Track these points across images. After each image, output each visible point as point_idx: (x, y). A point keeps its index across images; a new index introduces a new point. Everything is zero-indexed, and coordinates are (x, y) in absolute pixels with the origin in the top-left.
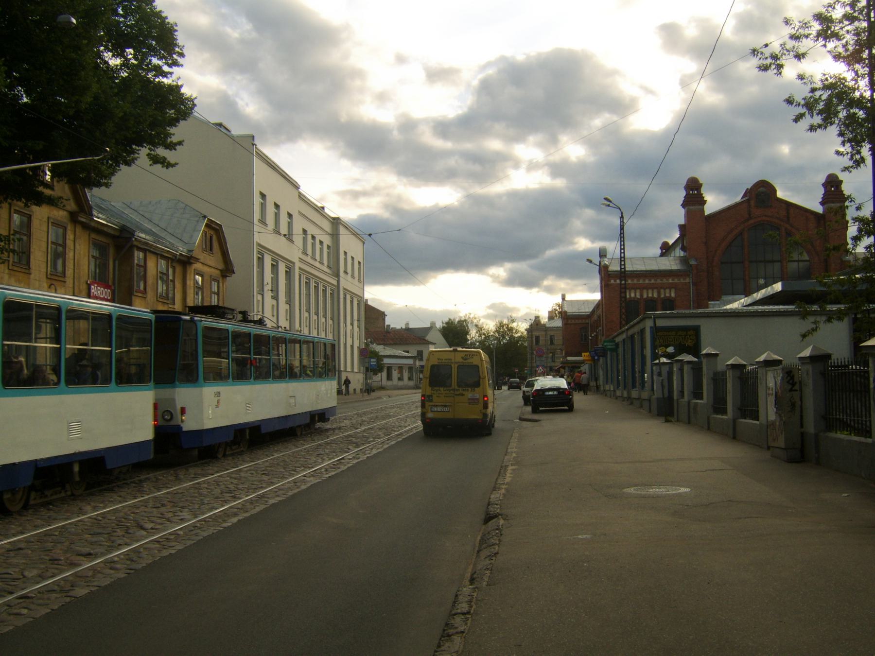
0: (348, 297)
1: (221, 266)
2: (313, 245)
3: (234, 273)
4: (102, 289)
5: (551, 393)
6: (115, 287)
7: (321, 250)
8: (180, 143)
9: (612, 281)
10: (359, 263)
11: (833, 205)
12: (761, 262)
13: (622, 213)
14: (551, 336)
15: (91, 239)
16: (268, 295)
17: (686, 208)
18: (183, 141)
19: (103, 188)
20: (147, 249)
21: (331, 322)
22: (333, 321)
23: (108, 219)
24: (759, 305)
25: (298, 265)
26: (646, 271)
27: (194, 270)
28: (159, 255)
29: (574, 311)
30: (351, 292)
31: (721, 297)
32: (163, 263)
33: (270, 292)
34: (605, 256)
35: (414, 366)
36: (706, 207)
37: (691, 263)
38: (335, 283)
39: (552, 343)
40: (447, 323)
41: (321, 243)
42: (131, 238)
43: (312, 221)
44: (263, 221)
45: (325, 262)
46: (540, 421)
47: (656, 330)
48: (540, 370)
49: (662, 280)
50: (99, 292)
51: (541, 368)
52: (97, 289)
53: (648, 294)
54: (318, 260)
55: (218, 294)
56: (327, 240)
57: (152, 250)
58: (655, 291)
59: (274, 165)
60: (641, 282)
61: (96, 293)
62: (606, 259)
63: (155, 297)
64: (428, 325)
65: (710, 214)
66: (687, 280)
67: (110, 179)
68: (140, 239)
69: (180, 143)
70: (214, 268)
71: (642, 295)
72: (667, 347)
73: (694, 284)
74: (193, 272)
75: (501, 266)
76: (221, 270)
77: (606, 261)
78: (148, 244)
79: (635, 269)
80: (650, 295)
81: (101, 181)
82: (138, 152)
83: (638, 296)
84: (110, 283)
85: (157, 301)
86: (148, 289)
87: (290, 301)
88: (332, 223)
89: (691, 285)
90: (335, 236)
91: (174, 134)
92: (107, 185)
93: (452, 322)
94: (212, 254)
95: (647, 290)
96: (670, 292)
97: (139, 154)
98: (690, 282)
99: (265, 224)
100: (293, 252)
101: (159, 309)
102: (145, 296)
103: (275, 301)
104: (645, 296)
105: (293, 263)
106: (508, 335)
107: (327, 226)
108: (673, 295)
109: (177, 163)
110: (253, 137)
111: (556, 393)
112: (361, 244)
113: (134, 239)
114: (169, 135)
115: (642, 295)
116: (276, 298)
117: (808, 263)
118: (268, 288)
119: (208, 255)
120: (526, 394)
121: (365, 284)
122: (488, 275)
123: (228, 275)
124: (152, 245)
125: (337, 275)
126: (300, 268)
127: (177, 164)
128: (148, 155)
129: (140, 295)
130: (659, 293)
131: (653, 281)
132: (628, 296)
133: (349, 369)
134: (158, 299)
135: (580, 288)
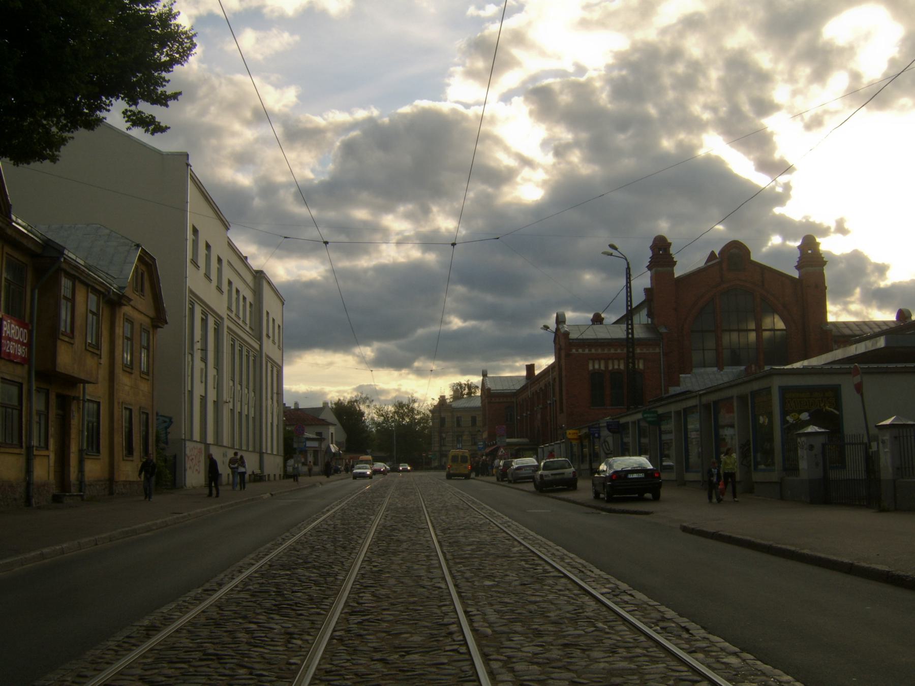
0: (269, 365)
1: (152, 313)
2: (238, 299)
3: (166, 323)
4: (17, 327)
5: (635, 476)
6: (32, 327)
7: (244, 306)
8: (175, 96)
9: (574, 351)
10: (279, 326)
13: (628, 264)
14: (458, 418)
15: (5, 255)
16: (198, 355)
17: (654, 270)
18: (180, 93)
19: (47, 162)
20: (78, 276)
21: (252, 394)
22: (255, 392)
23: (29, 228)
25: (227, 323)
26: (612, 339)
27: (124, 314)
28: (92, 287)
29: (505, 388)
30: (274, 361)
31: (692, 370)
32: (93, 298)
33: (200, 351)
34: (564, 322)
35: (319, 449)
36: (675, 268)
37: (660, 331)
38: (257, 347)
39: (459, 425)
40: (335, 404)
41: (244, 298)
42: (59, 258)
43: (237, 272)
44: (195, 263)
45: (248, 322)
46: (652, 513)
47: (784, 390)
48: (502, 452)
50: (13, 331)
51: (502, 449)
52: (10, 326)
53: (594, 366)
54: (242, 319)
55: (148, 349)
56: (250, 297)
57: (82, 278)
58: (622, 362)
59: (206, 194)
60: (606, 351)
61: (8, 332)
62: (565, 326)
63: (84, 345)
64: (321, 406)
66: (657, 350)
67: (58, 150)
68: (70, 260)
69: (175, 96)
70: (144, 314)
71: (606, 367)
72: (800, 412)
74: (122, 316)
75: (369, 345)
76: (152, 319)
77: (566, 328)
78: (79, 268)
79: (599, 337)
80: (616, 367)
81: (44, 152)
82: (108, 108)
83: (603, 367)
84: (27, 321)
85: (86, 349)
86: (77, 333)
87: (217, 365)
88: (255, 277)
89: (662, 356)
90: (258, 293)
91: (168, 81)
92: (54, 159)
93: (342, 403)
94: (143, 296)
97: (109, 111)
98: (660, 353)
99: (197, 267)
100: (219, 304)
102: (72, 342)
103: (204, 364)
104: (610, 368)
105: (222, 318)
106: (408, 416)
107: (249, 278)
109: (168, 126)
110: (188, 155)
111: (642, 475)
112: (281, 305)
113: (62, 260)
114: (162, 81)
115: (606, 367)
116: (204, 360)
117: (784, 332)
118: (198, 346)
119: (138, 297)
120: (545, 479)
122: (354, 355)
123: (160, 325)
124: (83, 271)
125: (260, 339)
126: (228, 328)
127: (167, 128)
128: (125, 113)
129: (67, 339)
132: (591, 368)
133: (269, 452)
134: (88, 348)
135: (452, 370)
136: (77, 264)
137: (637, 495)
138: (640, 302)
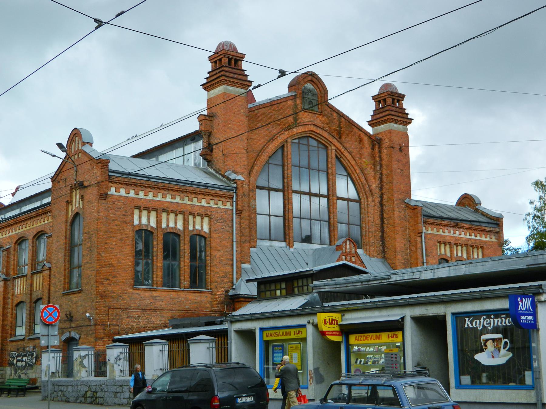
11: (230, 88)
12: (305, 193)
24: (142, 239)
49: (191, 200)
65: (290, 82)
66: (228, 206)
71: (159, 222)
73: (239, 213)
80: (172, 225)
95: (149, 212)
96: (202, 222)
101: (402, 126)
108: (206, 229)
115: (159, 222)
121: (311, 179)
130: (185, 222)
131: (177, 200)
132: (136, 222)
136: (360, 395)
137: (222, 407)
138: (58, 168)
